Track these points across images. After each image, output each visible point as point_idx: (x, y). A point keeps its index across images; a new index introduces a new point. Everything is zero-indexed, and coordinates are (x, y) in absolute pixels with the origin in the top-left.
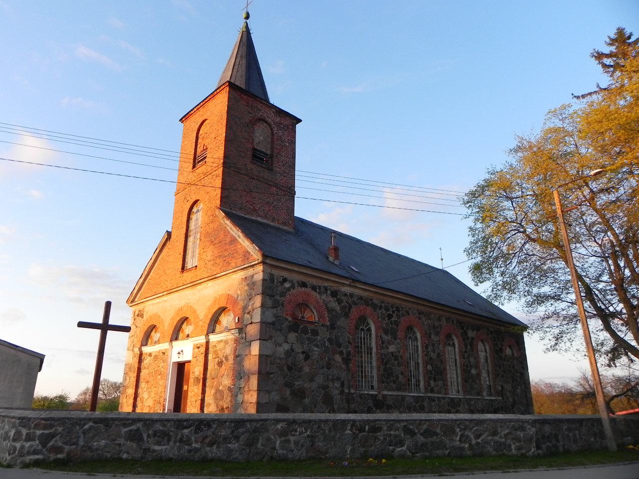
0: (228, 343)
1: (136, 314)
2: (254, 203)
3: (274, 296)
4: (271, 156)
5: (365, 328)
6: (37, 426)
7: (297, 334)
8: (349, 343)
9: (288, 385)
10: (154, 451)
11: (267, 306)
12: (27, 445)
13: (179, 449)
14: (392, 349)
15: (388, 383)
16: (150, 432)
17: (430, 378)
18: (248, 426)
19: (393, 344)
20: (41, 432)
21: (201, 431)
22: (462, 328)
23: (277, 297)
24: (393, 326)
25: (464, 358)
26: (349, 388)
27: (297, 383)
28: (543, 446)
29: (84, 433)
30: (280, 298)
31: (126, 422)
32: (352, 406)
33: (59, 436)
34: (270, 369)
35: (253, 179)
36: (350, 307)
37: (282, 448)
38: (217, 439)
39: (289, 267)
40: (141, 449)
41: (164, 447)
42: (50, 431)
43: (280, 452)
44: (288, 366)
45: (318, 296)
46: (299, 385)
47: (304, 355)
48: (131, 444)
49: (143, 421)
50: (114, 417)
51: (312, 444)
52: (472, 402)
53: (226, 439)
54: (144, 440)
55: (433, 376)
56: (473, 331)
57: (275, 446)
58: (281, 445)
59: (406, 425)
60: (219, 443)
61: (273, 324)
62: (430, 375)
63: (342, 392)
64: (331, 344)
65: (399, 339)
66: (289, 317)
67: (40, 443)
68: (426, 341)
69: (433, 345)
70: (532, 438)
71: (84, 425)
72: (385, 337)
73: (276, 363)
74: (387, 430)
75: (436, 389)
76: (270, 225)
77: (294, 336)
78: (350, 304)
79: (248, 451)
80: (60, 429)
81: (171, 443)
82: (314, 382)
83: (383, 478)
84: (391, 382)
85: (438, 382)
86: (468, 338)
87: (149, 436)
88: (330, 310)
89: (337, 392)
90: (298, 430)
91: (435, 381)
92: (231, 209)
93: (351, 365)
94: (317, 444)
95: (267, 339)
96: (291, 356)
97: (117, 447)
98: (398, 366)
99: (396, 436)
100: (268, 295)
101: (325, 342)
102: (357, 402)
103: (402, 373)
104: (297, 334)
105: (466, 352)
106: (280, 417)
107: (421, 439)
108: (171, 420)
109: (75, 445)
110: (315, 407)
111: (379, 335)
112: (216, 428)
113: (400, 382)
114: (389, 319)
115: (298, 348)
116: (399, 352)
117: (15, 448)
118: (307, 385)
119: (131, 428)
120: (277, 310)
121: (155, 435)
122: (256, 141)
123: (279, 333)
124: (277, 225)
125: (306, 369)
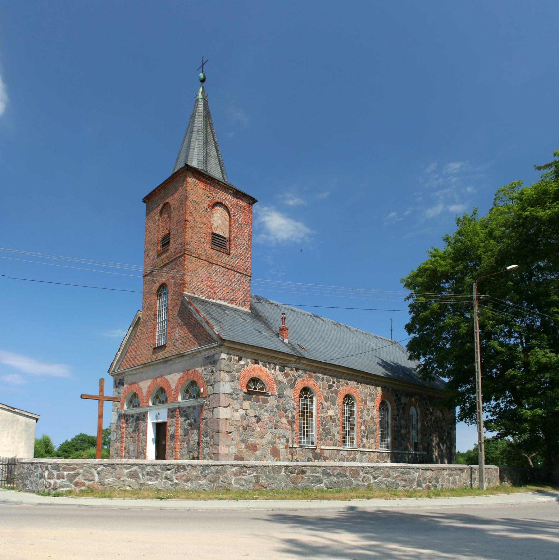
1: (117, 382)
3: (231, 372)
4: (229, 241)
5: (308, 396)
7: (250, 402)
8: (294, 408)
9: (243, 441)
10: (148, 485)
11: (225, 380)
12: (59, 481)
13: (165, 483)
15: (325, 440)
16: (144, 472)
17: (363, 436)
18: (213, 469)
19: (332, 409)
20: (68, 473)
21: (179, 472)
22: (397, 395)
24: (333, 394)
25: (395, 420)
27: (250, 440)
28: (423, 484)
29: (98, 473)
33: (81, 475)
35: (212, 263)
36: (296, 380)
37: (236, 483)
38: (191, 477)
41: (155, 482)
43: (235, 486)
46: (252, 441)
48: (131, 480)
50: (118, 462)
52: (400, 456)
53: (197, 477)
55: (366, 435)
56: (407, 397)
57: (231, 482)
58: (235, 481)
60: (192, 480)
61: (231, 394)
62: (363, 434)
63: (286, 447)
64: (279, 410)
65: (338, 405)
67: (68, 480)
68: (362, 407)
69: (368, 410)
70: (414, 479)
71: (98, 467)
73: (233, 424)
75: (367, 446)
77: (248, 403)
78: (295, 377)
79: (212, 485)
80: (81, 471)
81: (159, 480)
82: (264, 439)
83: (430, 557)
85: (370, 439)
86: (401, 404)
87: (143, 475)
88: (279, 383)
90: (247, 472)
91: (367, 438)
92: (194, 293)
93: (295, 426)
95: (226, 406)
96: (246, 419)
97: (122, 482)
99: (317, 477)
100: (227, 372)
103: (338, 433)
105: (398, 415)
106: (234, 463)
107: (335, 479)
108: (158, 465)
114: (329, 389)
115: (251, 413)
116: (337, 415)
117: (50, 484)
118: (258, 441)
120: (234, 383)
121: (148, 474)
122: (215, 226)
124: (235, 307)
125: (258, 429)
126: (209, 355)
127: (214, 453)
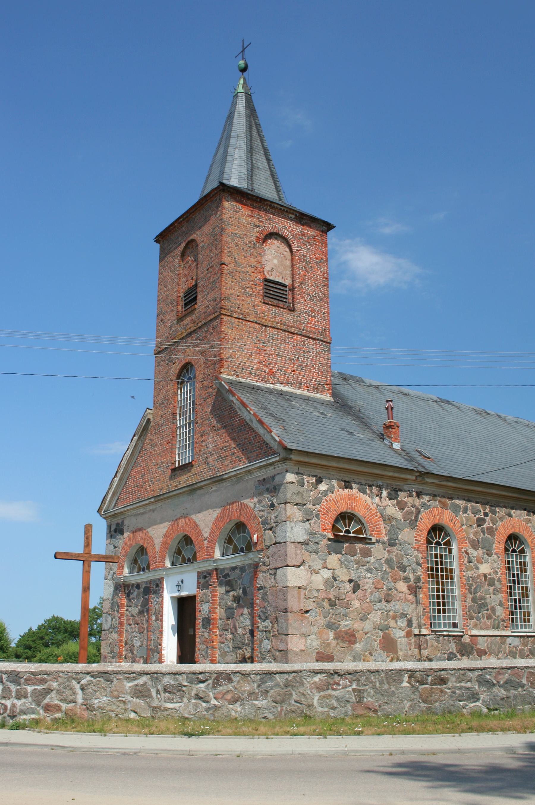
0: (245, 571)
1: (113, 529)
2: (270, 363)
3: (305, 505)
4: (293, 289)
6: (28, 681)
7: (339, 556)
9: (330, 626)
10: (166, 709)
11: (295, 520)
12: (19, 703)
13: (196, 706)
14: (484, 569)
15: (478, 619)
16: (160, 687)
19: (487, 561)
20: (33, 688)
21: (220, 686)
23: (310, 506)
24: (486, 535)
26: (419, 626)
27: (343, 623)
29: (82, 689)
30: (314, 507)
31: (129, 675)
32: (425, 653)
33: (54, 692)
34: (304, 606)
35: (266, 326)
36: (419, 512)
39: (324, 462)
40: (150, 706)
41: (177, 705)
42: (43, 687)
43: (320, 709)
44: (329, 600)
45: (369, 500)
46: (346, 625)
47: (352, 584)
49: (149, 674)
50: (115, 669)
51: (360, 700)
53: (252, 695)
54: (152, 697)
57: (313, 703)
58: (320, 701)
59: (481, 675)
60: (242, 700)
61: (306, 543)
63: (409, 634)
64: (391, 567)
65: (496, 554)
66: (328, 532)
67: (34, 701)
71: (82, 678)
72: (474, 553)
73: (312, 597)
74: (456, 681)
76: (296, 394)
77: (336, 558)
78: (417, 509)
79: (279, 709)
80: (55, 685)
82: (368, 621)
84: (483, 618)
88: (388, 519)
89: (403, 634)
90: (341, 683)
92: (237, 376)
93: (421, 596)
94: (365, 700)
95: (298, 564)
97: (122, 705)
98: (494, 594)
101: (381, 565)
102: (432, 646)
104: (341, 555)
106: (317, 668)
107: (502, 692)
108: (183, 673)
109: (73, 702)
110: (371, 654)
111: (463, 550)
112: (239, 682)
113: (498, 616)
114: (479, 526)
115: (343, 575)
116: (496, 573)
118: (357, 625)
119: (136, 682)
122: (268, 268)
123: (314, 556)
125: (356, 604)
126: (265, 477)
127: (280, 649)
